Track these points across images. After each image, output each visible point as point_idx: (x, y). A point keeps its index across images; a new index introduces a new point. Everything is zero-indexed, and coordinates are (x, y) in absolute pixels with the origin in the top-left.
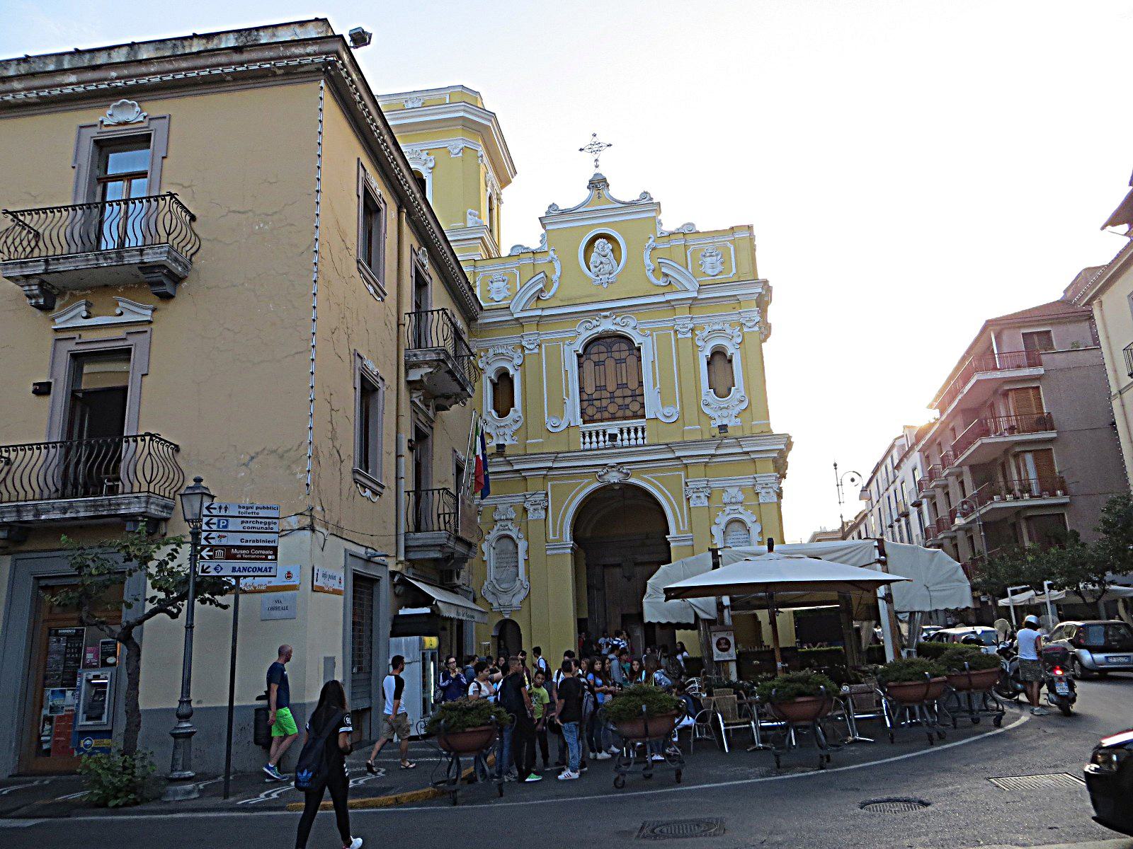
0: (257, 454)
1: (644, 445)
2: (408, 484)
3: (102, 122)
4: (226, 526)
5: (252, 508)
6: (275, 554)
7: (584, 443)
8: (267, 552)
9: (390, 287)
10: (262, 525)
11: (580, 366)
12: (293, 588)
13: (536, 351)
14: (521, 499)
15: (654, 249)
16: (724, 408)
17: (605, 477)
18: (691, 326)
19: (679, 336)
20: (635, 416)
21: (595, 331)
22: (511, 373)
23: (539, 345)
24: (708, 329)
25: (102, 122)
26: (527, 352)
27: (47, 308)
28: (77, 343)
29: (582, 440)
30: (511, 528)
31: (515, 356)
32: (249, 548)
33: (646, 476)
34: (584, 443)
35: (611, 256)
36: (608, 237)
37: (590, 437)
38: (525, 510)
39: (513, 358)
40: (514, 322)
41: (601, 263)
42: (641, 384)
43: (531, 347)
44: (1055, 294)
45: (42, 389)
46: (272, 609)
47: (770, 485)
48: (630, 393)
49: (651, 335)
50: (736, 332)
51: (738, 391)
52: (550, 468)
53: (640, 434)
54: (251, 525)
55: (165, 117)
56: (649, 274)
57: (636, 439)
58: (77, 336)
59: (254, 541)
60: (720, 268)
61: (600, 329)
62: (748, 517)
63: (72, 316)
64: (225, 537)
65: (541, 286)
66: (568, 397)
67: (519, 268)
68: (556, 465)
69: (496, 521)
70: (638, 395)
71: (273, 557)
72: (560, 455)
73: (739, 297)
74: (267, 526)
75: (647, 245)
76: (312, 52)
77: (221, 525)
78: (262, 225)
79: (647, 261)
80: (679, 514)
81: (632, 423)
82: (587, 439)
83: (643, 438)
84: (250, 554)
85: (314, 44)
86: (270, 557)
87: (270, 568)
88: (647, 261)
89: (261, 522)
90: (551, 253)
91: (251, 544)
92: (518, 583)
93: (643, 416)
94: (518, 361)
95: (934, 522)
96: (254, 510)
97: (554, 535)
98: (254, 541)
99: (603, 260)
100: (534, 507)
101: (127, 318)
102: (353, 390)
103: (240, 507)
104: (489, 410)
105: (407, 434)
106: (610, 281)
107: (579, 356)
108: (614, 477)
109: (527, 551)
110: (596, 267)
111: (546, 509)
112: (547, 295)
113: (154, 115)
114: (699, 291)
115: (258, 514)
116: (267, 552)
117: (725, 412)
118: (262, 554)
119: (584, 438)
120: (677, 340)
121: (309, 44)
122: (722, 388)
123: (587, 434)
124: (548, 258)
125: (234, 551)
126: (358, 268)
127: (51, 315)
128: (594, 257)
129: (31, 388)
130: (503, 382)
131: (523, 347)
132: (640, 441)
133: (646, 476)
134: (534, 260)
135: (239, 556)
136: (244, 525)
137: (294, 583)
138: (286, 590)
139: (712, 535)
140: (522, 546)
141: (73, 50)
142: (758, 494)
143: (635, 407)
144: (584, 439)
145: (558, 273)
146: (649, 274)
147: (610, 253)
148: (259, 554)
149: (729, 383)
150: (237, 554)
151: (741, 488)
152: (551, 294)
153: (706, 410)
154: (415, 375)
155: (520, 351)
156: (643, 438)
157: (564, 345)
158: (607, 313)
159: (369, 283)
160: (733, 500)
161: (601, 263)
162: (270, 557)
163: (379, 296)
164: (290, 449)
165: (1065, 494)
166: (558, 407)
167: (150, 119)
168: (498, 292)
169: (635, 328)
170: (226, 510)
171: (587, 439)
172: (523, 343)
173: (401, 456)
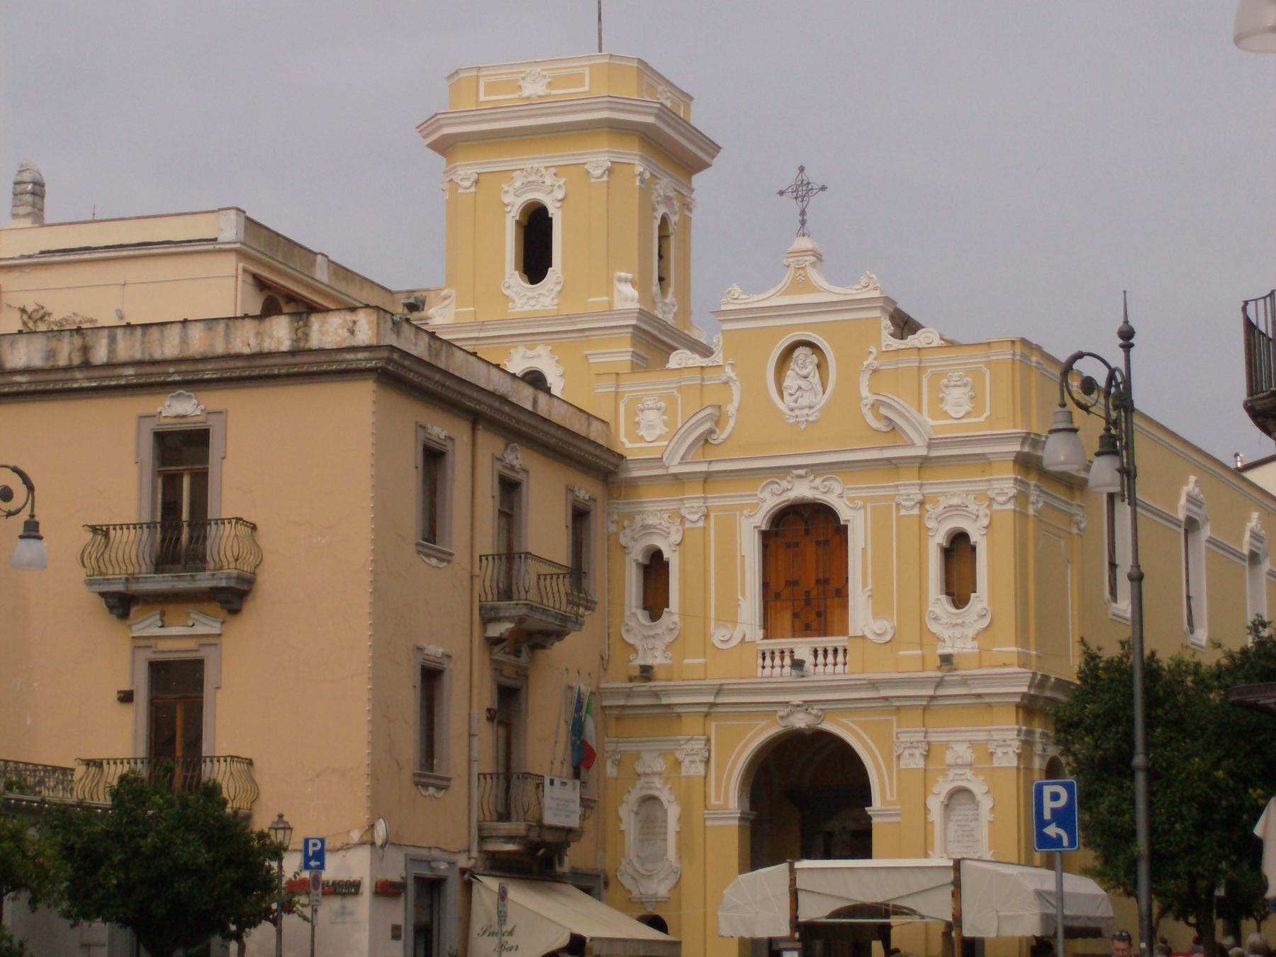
3: (160, 413)
11: (765, 547)
13: (701, 524)
15: (875, 371)
16: (957, 625)
18: (920, 497)
22: (666, 556)
23: (706, 516)
24: (943, 502)
25: (160, 413)
27: (124, 615)
28: (155, 652)
29: (760, 661)
31: (673, 529)
33: (844, 720)
35: (815, 379)
39: (669, 533)
41: (800, 388)
43: (694, 518)
45: (126, 697)
47: (1008, 742)
49: (864, 507)
50: (983, 511)
53: (840, 658)
55: (221, 412)
56: (866, 411)
58: (154, 645)
63: (147, 625)
65: (707, 426)
69: (639, 775)
73: (989, 456)
76: (363, 358)
79: (865, 392)
80: (885, 773)
82: (768, 661)
83: (845, 664)
85: (363, 351)
88: (865, 392)
90: (728, 369)
94: (676, 538)
97: (717, 798)
99: (802, 383)
101: (200, 629)
104: (634, 610)
108: (800, 721)
110: (791, 395)
112: (721, 436)
113: (210, 408)
117: (958, 632)
119: (764, 659)
120: (899, 519)
121: (359, 351)
124: (724, 378)
127: (128, 623)
128: (790, 381)
129: (116, 696)
130: (655, 567)
131: (683, 519)
134: (703, 379)
140: (673, 812)
141: (125, 324)
142: (992, 754)
146: (866, 411)
151: (972, 744)
153: (934, 627)
154: (496, 630)
155: (678, 521)
158: (802, 472)
160: (960, 761)
161: (800, 388)
166: (729, 616)
167: (209, 413)
168: (651, 427)
169: (841, 496)
171: (768, 661)
172: (683, 512)
173: (474, 735)
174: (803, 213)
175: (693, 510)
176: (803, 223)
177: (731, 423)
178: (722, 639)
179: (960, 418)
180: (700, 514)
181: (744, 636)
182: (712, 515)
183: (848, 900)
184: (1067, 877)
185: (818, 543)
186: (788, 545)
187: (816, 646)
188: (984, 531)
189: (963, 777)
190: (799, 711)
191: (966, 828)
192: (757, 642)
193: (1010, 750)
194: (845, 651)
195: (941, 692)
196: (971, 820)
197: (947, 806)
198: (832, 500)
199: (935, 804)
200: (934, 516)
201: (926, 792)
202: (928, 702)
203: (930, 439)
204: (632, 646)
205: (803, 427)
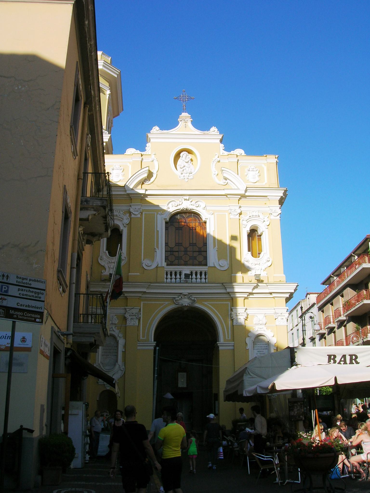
1: (206, 283)
4: (7, 291)
5: (27, 279)
6: (42, 318)
7: (167, 279)
8: (36, 316)
10: (33, 294)
11: (167, 229)
12: (28, 349)
13: (139, 216)
14: (122, 311)
17: (179, 301)
18: (239, 211)
19: (232, 217)
20: (200, 264)
23: (142, 213)
26: (133, 216)
29: (165, 276)
30: (114, 329)
31: (125, 218)
33: (205, 303)
34: (167, 279)
37: (171, 275)
38: (125, 319)
40: (125, 196)
48: (197, 249)
52: (145, 293)
53: (203, 276)
54: (25, 293)
57: (201, 279)
59: (26, 306)
60: (257, 179)
64: (6, 300)
66: (158, 248)
68: (148, 291)
71: (40, 320)
72: (152, 284)
74: (37, 295)
75: (214, 159)
77: (3, 289)
78: (20, 87)
81: (199, 269)
84: (23, 316)
89: (32, 292)
92: (117, 366)
94: (126, 221)
96: (28, 281)
97: (143, 337)
98: (26, 306)
100: (132, 317)
103: (17, 277)
106: (190, 178)
107: (166, 223)
108: (186, 302)
109: (125, 346)
111: (139, 320)
114: (246, 191)
115: (31, 284)
118: (32, 317)
119: (167, 275)
123: (173, 273)
124: (151, 160)
125: (11, 312)
129: (22, 424)
131: (130, 213)
132: (203, 280)
133: (205, 303)
135: (15, 316)
136: (20, 292)
137: (28, 346)
138: (19, 351)
140: (121, 342)
143: (200, 258)
145: (157, 169)
150: (13, 315)
155: (128, 215)
156: (205, 279)
159: (73, 144)
160: (260, 322)
162: (38, 320)
166: (151, 255)
170: (7, 278)
171: (169, 276)
175: (136, 210)
179: (254, 183)
180: (139, 212)
181: (158, 265)
182: (144, 213)
183: (291, 388)
187: (192, 270)
188: (267, 227)
190: (185, 298)
191: (262, 353)
192: (165, 267)
193: (284, 318)
194: (205, 273)
195: (255, 291)
196: (264, 349)
200: (245, 220)
202: (248, 295)
203: (247, 187)
204: (103, 266)
205: (187, 180)
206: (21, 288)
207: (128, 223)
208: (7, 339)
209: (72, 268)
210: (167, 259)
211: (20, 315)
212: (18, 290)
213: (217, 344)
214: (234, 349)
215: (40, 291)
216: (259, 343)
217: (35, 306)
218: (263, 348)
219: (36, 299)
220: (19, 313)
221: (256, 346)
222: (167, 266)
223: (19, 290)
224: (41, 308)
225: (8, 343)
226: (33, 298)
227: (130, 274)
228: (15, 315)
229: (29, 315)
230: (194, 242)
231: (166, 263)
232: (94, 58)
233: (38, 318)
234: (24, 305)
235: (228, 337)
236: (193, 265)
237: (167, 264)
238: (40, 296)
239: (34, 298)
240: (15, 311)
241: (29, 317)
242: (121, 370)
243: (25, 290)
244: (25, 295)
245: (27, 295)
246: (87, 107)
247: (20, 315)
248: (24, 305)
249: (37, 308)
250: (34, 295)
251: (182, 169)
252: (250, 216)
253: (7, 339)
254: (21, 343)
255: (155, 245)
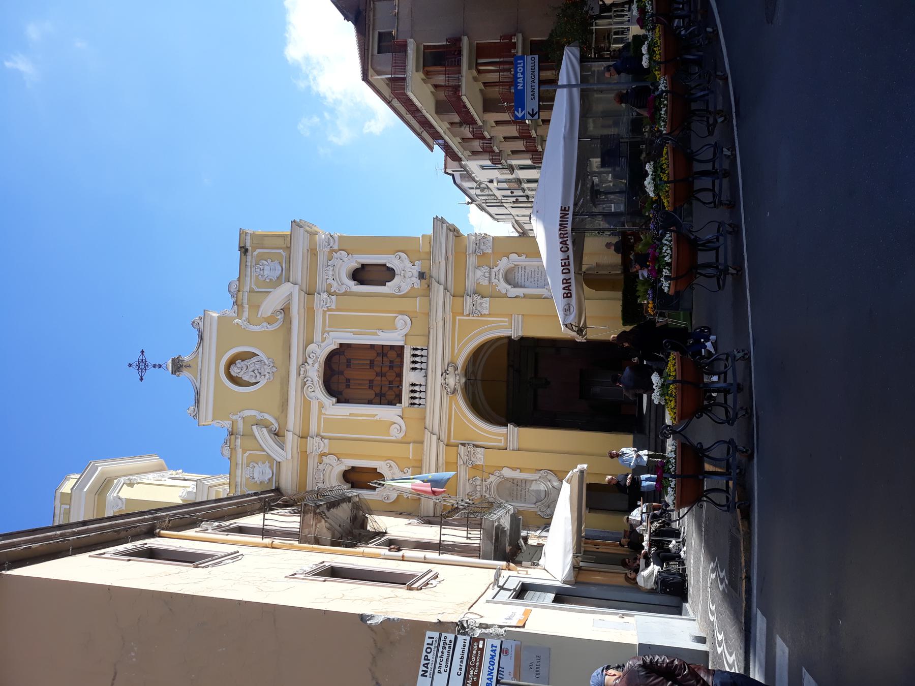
0: (373, 678)
2: (432, 555)
8: (475, 648)
9: (230, 549)
10: (446, 651)
11: (347, 401)
19: (333, 307)
21: (316, 383)
23: (322, 437)
32: (468, 667)
36: (231, 363)
41: (253, 371)
42: (372, 346)
44: (350, 27)
46: (538, 673)
48: (379, 359)
51: (392, 261)
54: (444, 663)
59: (462, 662)
61: (316, 379)
62: (504, 264)
67: (244, 451)
70: (383, 351)
71: (481, 642)
74: (447, 646)
78: (133, 654)
83: (422, 349)
84: (474, 666)
86: (481, 646)
87: (492, 646)
89: (443, 652)
91: (464, 665)
93: (402, 347)
95: (528, 155)
98: (462, 662)
102: (326, 582)
105: (385, 551)
107: (338, 402)
116: (475, 648)
118: (477, 654)
119: (415, 404)
120: (338, 310)
122: (384, 274)
126: (203, 567)
135: (475, 678)
136: (442, 671)
139: (516, 297)
143: (392, 355)
144: (416, 398)
147: (245, 362)
148: (476, 657)
149: (384, 268)
152: (273, 421)
157: (325, 414)
160: (487, 275)
161: (253, 371)
162: (481, 646)
163: (237, 557)
164: (375, 640)
165: (515, 35)
171: (417, 401)
174: (154, 366)
176: (160, 366)
177: (267, 416)
178: (399, 431)
184: (560, 83)
185: (348, 366)
186: (348, 386)
189: (497, 274)
194: (414, 349)
196: (525, 272)
197: (516, 286)
198: (323, 354)
199: (514, 292)
201: (505, 296)
206: (437, 669)
207: (336, 458)
208: (503, 675)
209: (403, 559)
210: (391, 403)
211: (474, 671)
212: (440, 673)
213: (514, 338)
214: (523, 315)
215: (442, 639)
216: (516, 279)
217: (462, 649)
218: (523, 272)
219: (452, 648)
220: (471, 673)
221: (519, 283)
222: (401, 403)
223: (439, 672)
224: (465, 641)
225: (509, 675)
226: (451, 652)
227: (411, 458)
228: (473, 679)
229: (474, 658)
230: (368, 362)
231: (397, 405)
232: (99, 548)
233: (478, 645)
234: (460, 666)
235: (506, 322)
236: (401, 366)
237: (399, 403)
238: (448, 642)
239: (451, 650)
240: (468, 679)
241: (476, 660)
242: (547, 475)
243: (440, 664)
244: (446, 663)
245: (447, 661)
246: (159, 532)
247: (474, 671)
248: (460, 666)
249: (464, 646)
250: (447, 649)
251: (258, 375)
252: (333, 279)
253: (503, 675)
254: (510, 655)
255: (372, 418)
